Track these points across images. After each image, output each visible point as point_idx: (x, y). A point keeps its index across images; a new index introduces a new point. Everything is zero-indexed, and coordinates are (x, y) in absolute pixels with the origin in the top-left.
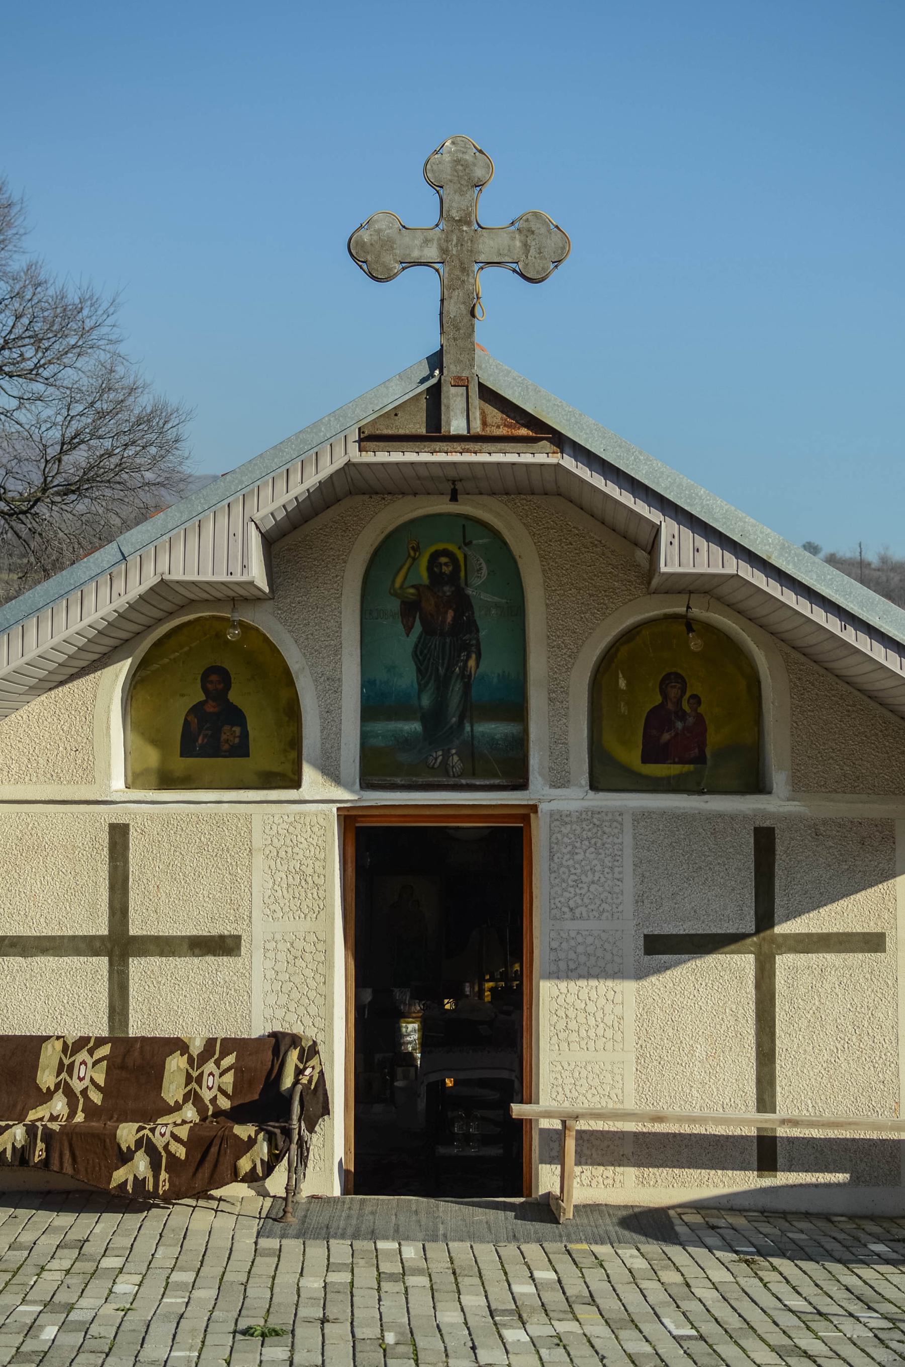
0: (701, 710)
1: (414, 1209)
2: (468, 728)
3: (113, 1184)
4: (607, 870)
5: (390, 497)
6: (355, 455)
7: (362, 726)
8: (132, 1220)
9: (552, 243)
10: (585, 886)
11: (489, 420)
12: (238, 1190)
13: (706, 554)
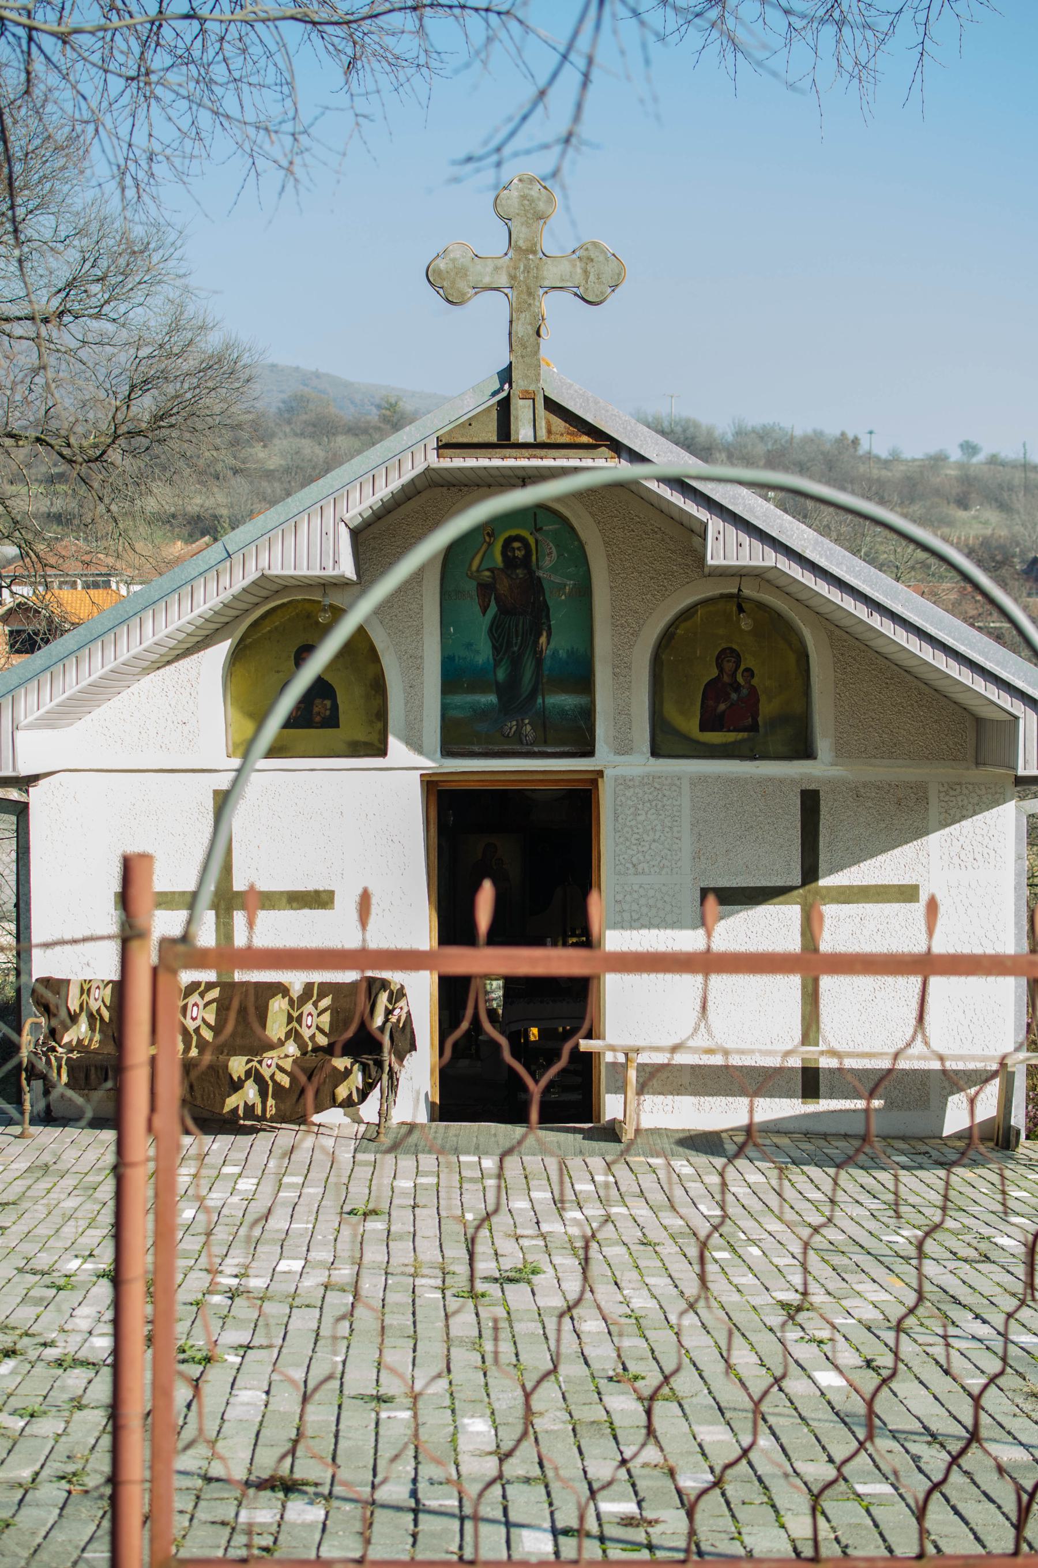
0: (754, 682)
1: (493, 1132)
2: (540, 700)
3: (226, 1109)
4: (667, 829)
5: (466, 489)
6: (434, 461)
7: (442, 699)
8: (244, 1140)
9: (609, 270)
10: (647, 844)
11: (554, 429)
12: (333, 1117)
13: (748, 548)
